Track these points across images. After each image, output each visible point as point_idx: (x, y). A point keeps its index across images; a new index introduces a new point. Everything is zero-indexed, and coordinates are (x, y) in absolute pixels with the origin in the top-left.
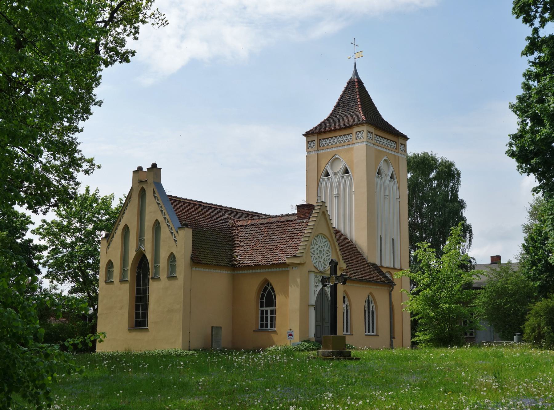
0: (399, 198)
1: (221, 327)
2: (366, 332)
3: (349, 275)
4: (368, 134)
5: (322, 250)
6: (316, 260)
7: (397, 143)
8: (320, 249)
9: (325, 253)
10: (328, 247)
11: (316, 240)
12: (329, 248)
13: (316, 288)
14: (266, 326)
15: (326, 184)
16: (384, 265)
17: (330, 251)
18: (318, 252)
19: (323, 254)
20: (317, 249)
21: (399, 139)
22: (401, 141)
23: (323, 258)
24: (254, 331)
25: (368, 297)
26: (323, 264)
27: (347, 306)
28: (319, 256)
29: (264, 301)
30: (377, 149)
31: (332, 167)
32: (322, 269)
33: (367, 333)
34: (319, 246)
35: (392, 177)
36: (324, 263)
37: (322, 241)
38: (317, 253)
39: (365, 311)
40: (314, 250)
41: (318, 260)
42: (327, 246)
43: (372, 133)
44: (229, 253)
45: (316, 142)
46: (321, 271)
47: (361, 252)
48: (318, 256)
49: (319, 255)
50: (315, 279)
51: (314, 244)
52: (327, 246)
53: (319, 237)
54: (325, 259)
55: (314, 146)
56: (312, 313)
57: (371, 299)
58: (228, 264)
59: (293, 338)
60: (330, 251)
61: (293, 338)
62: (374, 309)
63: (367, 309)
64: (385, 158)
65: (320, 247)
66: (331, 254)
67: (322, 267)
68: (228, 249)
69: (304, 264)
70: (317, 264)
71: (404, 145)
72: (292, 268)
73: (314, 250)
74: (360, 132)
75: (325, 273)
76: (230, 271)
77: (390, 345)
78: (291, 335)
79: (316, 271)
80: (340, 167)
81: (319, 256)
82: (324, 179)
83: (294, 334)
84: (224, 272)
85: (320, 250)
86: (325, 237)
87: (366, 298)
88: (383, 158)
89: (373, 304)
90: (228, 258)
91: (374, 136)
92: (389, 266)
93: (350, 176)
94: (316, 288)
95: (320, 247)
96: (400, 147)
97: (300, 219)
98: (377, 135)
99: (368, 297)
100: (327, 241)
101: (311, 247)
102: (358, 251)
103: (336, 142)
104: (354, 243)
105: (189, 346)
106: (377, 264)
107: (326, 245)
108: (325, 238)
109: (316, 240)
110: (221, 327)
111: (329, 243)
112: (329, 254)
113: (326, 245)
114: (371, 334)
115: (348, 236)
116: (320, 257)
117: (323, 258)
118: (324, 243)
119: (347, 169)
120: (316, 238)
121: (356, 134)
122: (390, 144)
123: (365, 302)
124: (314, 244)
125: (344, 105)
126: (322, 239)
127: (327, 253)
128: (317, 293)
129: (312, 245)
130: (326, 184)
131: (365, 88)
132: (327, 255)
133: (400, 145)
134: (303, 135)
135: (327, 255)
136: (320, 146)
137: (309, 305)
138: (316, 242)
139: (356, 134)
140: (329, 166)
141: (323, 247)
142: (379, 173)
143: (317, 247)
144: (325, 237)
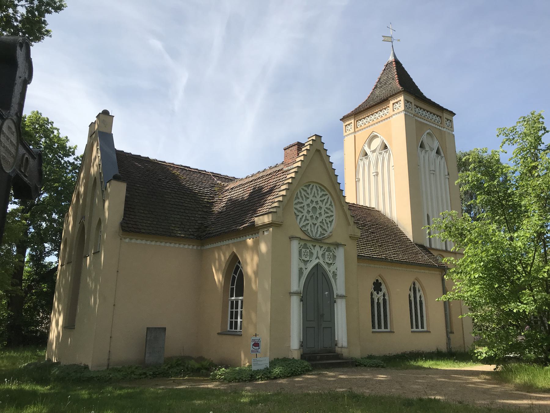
0: (448, 174)
1: (164, 329)
2: (412, 328)
3: (385, 256)
4: (406, 103)
5: (318, 207)
6: (307, 222)
7: (442, 117)
8: (314, 204)
9: (323, 213)
10: (329, 203)
11: (305, 191)
12: (330, 205)
13: (306, 264)
14: (236, 328)
15: (364, 164)
16: (433, 246)
17: (334, 209)
18: (310, 209)
19: (320, 214)
20: (308, 205)
21: (444, 114)
22: (445, 115)
23: (320, 220)
24: (218, 334)
25: (414, 284)
26: (320, 229)
27: (384, 295)
28: (312, 217)
29: (235, 287)
30: (418, 120)
31: (369, 147)
32: (318, 235)
33: (415, 329)
34: (308, 205)
35: (438, 152)
36: (321, 226)
37: (318, 194)
38: (308, 212)
39: (410, 301)
40: (302, 205)
41: (310, 222)
42: (326, 203)
43: (411, 103)
44: (199, 222)
45: (353, 125)
46: (315, 239)
47: (404, 232)
48: (310, 215)
49: (311, 214)
50: (303, 250)
51: (302, 197)
52: (326, 203)
53: (311, 186)
54: (324, 221)
55: (351, 128)
56: (295, 304)
57: (417, 286)
58: (193, 235)
59: (259, 350)
60: (334, 209)
61: (259, 350)
62: (423, 299)
63: (412, 299)
64: (428, 131)
65: (314, 203)
66: (334, 214)
67: (319, 233)
68: (199, 216)
69: (281, 225)
70: (308, 227)
71: (451, 121)
72: (262, 232)
73: (302, 205)
74: (397, 103)
75: (322, 241)
76: (198, 246)
77: (447, 343)
78: (256, 345)
79: (306, 238)
80: (376, 143)
81: (312, 217)
82: (361, 160)
83: (262, 344)
84: (186, 246)
85: (314, 207)
86: (323, 188)
87: (410, 284)
88: (427, 130)
89: (421, 292)
90: (195, 228)
91: (414, 107)
92: (438, 247)
93: (388, 151)
94: (306, 264)
95: (314, 203)
96: (445, 122)
97: (287, 167)
98: (417, 107)
99: (414, 284)
100: (313, 185)
101: (296, 201)
102: (400, 231)
103: (373, 119)
104: (396, 223)
105: (109, 359)
106: (425, 245)
107: (326, 201)
108: (322, 190)
109: (305, 191)
110: (164, 329)
111: (330, 199)
112: (331, 214)
113: (326, 201)
114: (420, 329)
115: (382, 212)
116: (315, 217)
117: (320, 220)
118: (321, 197)
119: (386, 145)
120: (305, 188)
121: (393, 106)
122: (434, 118)
123: (410, 290)
124: (302, 197)
125: (382, 85)
126: (317, 190)
127: (327, 213)
128: (306, 273)
129: (299, 199)
130: (364, 164)
131: (403, 68)
132: (326, 215)
133: (445, 120)
134: (341, 120)
135: (326, 215)
136: (357, 127)
137: (290, 293)
138: (306, 195)
139: (393, 106)
140: (366, 145)
141: (319, 202)
142: (422, 146)
143: (309, 201)
144: (323, 188)
